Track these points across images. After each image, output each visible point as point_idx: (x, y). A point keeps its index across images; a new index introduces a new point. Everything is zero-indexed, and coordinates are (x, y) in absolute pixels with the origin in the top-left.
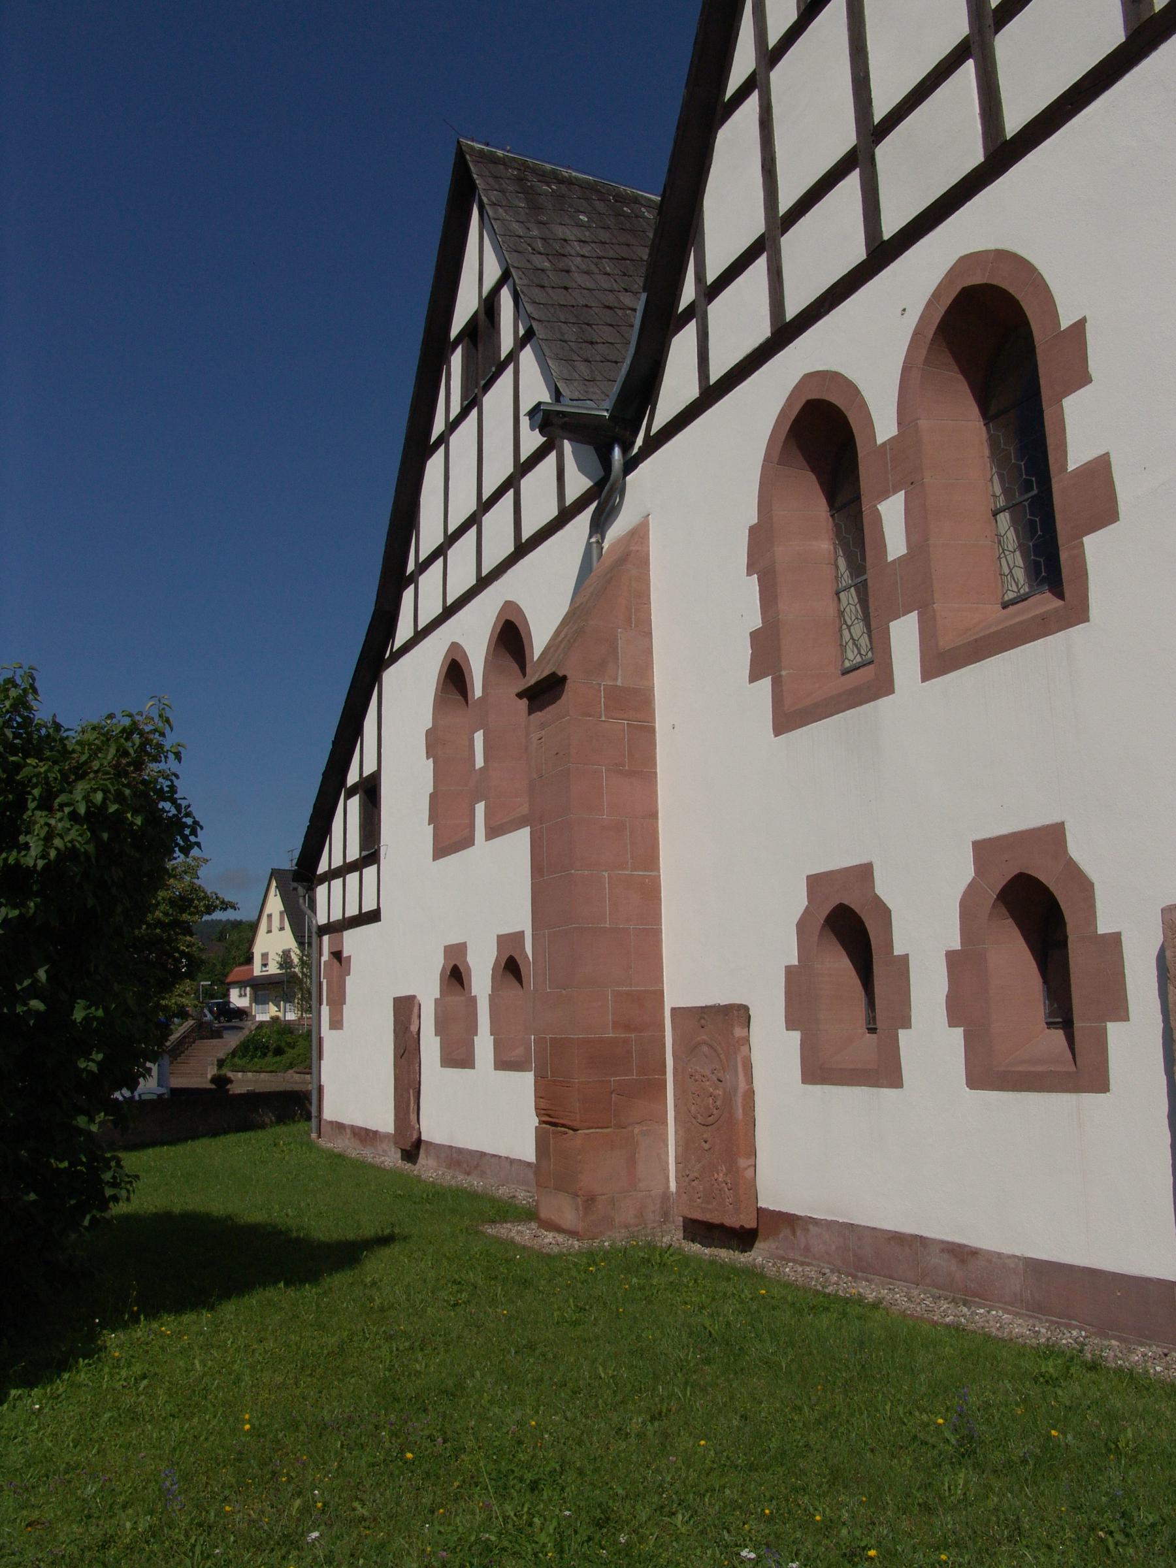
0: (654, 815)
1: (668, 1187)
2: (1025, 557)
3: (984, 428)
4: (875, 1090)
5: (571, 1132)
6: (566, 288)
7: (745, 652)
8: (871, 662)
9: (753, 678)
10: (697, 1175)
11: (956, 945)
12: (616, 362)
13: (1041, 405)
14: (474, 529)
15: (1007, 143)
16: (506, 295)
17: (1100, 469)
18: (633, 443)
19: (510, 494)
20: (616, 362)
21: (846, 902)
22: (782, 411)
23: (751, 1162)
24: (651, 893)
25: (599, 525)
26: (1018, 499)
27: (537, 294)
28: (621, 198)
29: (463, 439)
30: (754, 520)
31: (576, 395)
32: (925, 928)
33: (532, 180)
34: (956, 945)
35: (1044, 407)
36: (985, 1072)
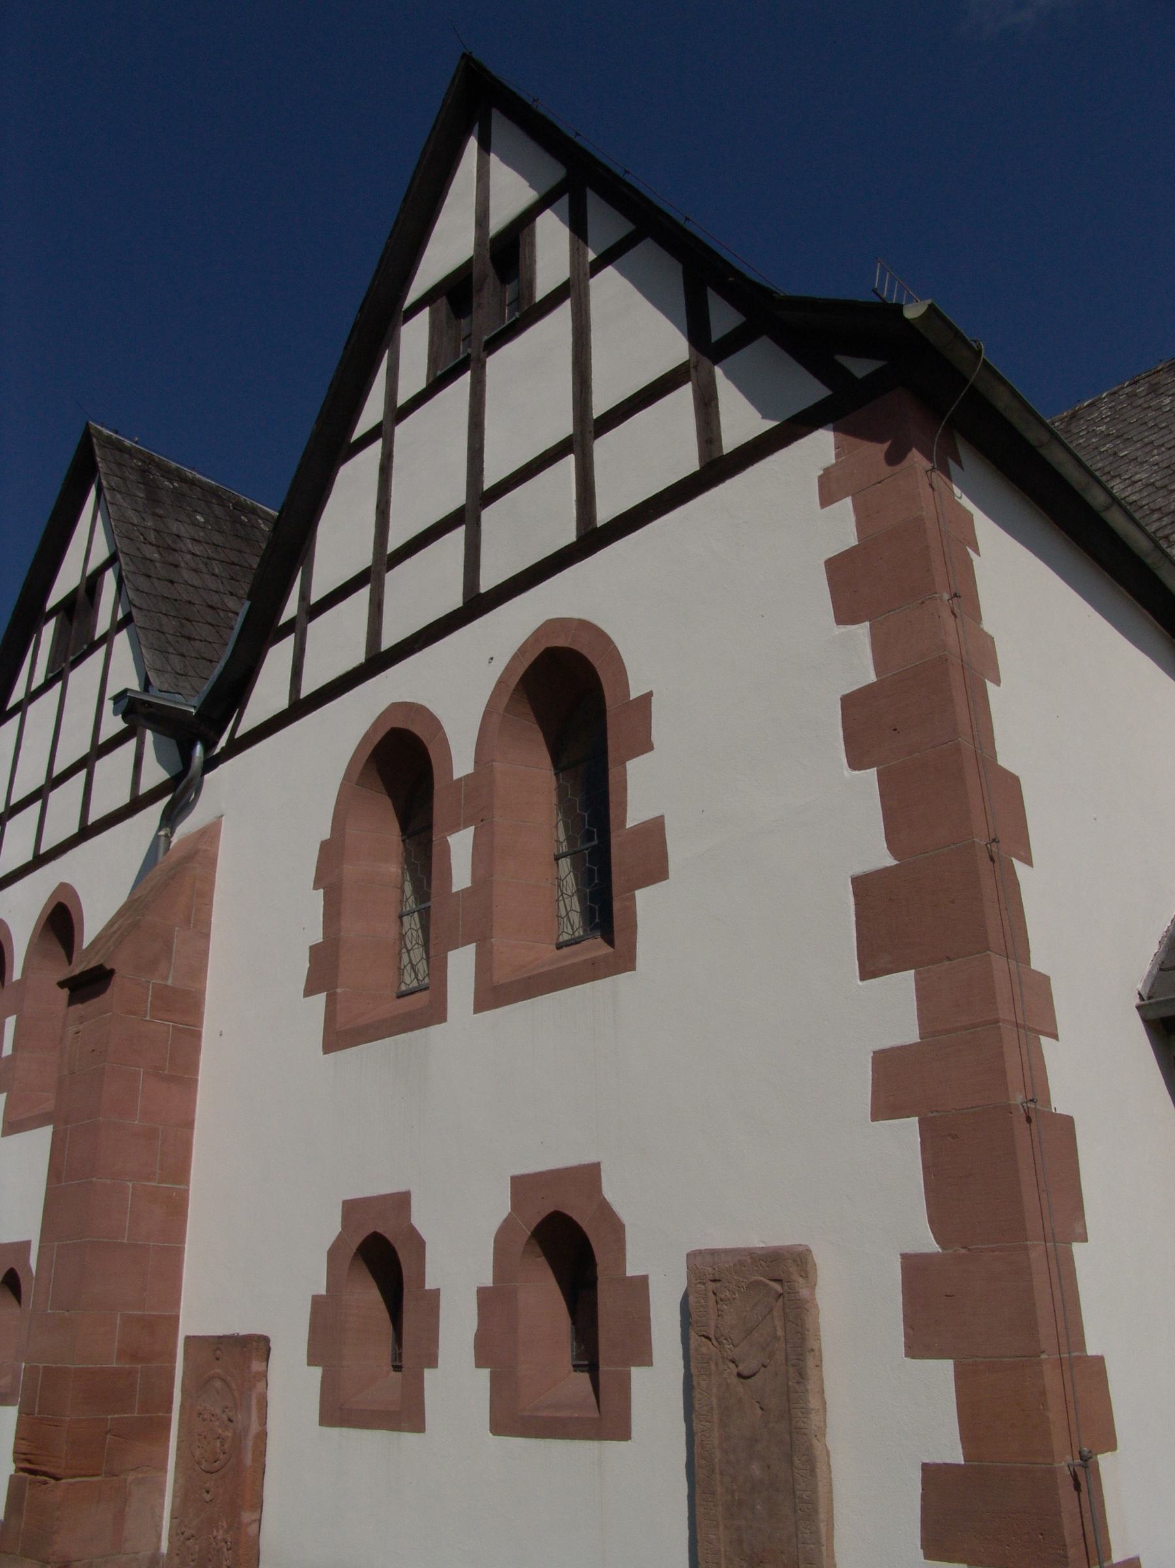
0: (190, 1125)
1: (158, 1548)
2: (581, 902)
3: (554, 778)
4: (395, 1434)
5: (52, 1481)
6: (172, 582)
7: (303, 965)
8: (426, 989)
9: (309, 991)
10: (192, 1532)
11: (488, 1281)
12: (211, 661)
13: (607, 763)
14: (39, 804)
15: (596, 530)
16: (110, 578)
17: (655, 829)
18: (216, 743)
19: (83, 774)
20: (211, 661)
21: (379, 1231)
22: (367, 734)
23: (255, 1516)
24: (177, 1208)
25: (170, 819)
26: (580, 847)
27: (143, 583)
28: (240, 507)
29: (42, 711)
30: (327, 835)
31: (165, 687)
32: (459, 1262)
33: (156, 475)
34: (488, 1281)
35: (610, 765)
36: (512, 1417)
